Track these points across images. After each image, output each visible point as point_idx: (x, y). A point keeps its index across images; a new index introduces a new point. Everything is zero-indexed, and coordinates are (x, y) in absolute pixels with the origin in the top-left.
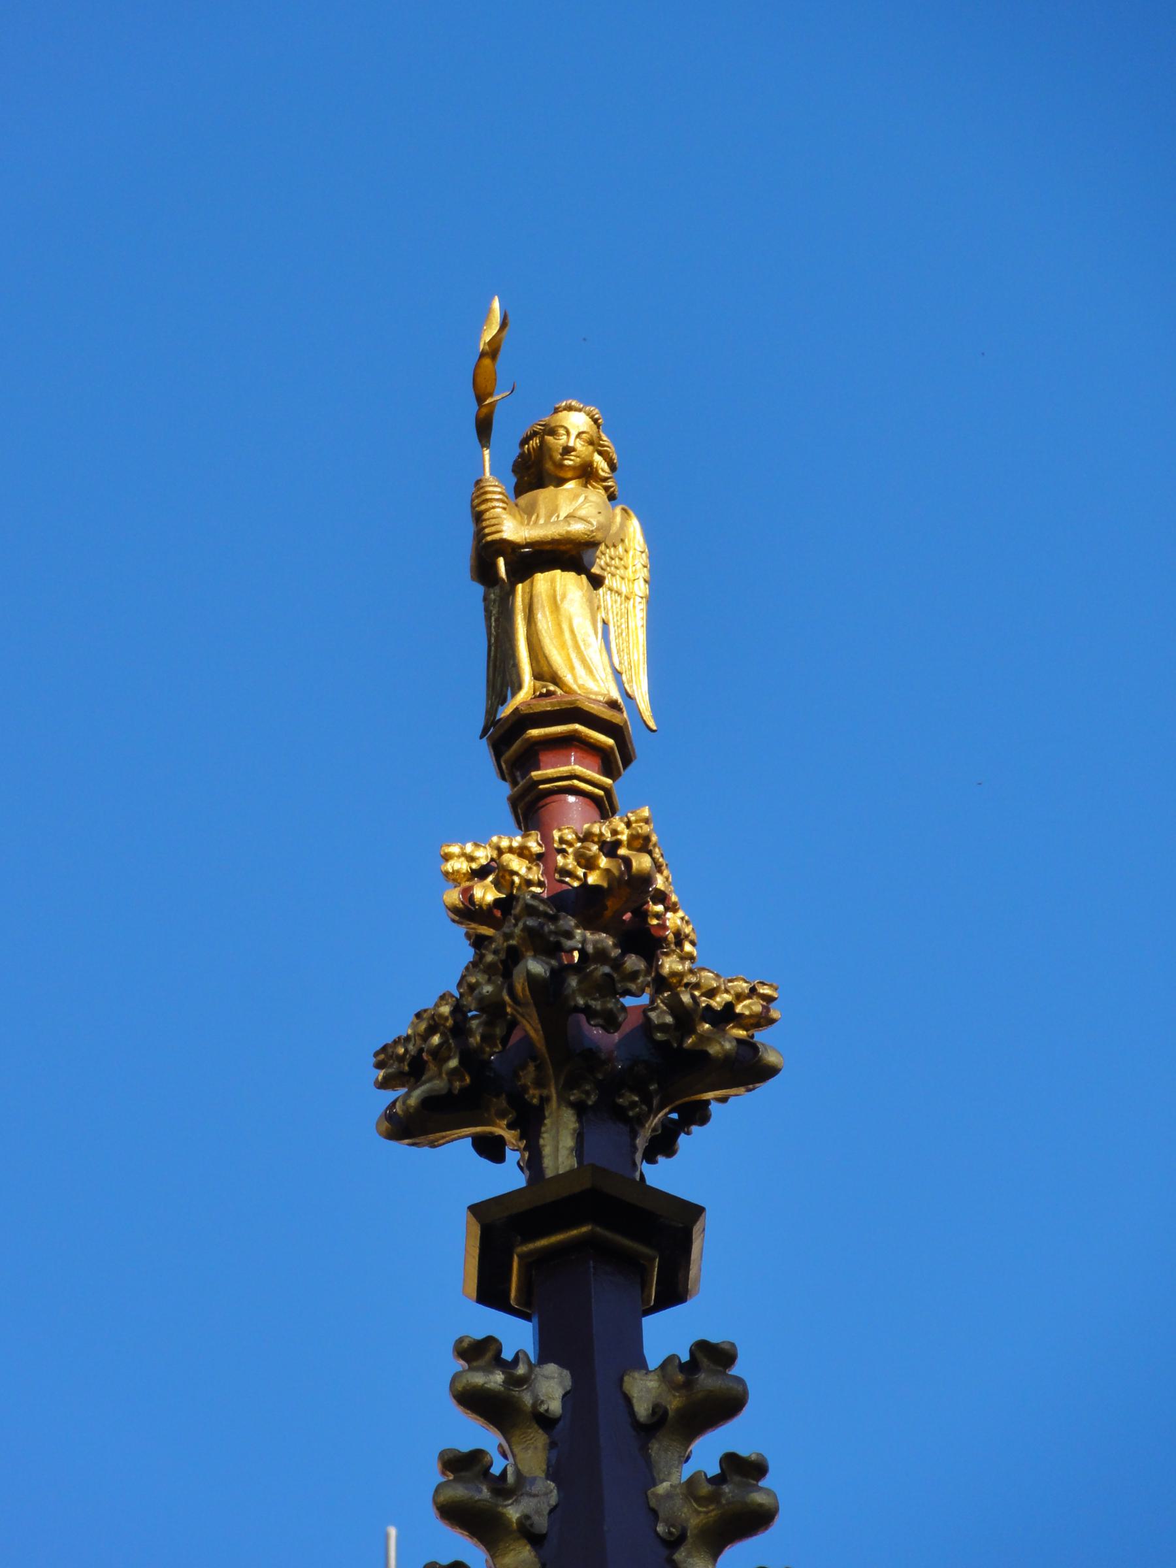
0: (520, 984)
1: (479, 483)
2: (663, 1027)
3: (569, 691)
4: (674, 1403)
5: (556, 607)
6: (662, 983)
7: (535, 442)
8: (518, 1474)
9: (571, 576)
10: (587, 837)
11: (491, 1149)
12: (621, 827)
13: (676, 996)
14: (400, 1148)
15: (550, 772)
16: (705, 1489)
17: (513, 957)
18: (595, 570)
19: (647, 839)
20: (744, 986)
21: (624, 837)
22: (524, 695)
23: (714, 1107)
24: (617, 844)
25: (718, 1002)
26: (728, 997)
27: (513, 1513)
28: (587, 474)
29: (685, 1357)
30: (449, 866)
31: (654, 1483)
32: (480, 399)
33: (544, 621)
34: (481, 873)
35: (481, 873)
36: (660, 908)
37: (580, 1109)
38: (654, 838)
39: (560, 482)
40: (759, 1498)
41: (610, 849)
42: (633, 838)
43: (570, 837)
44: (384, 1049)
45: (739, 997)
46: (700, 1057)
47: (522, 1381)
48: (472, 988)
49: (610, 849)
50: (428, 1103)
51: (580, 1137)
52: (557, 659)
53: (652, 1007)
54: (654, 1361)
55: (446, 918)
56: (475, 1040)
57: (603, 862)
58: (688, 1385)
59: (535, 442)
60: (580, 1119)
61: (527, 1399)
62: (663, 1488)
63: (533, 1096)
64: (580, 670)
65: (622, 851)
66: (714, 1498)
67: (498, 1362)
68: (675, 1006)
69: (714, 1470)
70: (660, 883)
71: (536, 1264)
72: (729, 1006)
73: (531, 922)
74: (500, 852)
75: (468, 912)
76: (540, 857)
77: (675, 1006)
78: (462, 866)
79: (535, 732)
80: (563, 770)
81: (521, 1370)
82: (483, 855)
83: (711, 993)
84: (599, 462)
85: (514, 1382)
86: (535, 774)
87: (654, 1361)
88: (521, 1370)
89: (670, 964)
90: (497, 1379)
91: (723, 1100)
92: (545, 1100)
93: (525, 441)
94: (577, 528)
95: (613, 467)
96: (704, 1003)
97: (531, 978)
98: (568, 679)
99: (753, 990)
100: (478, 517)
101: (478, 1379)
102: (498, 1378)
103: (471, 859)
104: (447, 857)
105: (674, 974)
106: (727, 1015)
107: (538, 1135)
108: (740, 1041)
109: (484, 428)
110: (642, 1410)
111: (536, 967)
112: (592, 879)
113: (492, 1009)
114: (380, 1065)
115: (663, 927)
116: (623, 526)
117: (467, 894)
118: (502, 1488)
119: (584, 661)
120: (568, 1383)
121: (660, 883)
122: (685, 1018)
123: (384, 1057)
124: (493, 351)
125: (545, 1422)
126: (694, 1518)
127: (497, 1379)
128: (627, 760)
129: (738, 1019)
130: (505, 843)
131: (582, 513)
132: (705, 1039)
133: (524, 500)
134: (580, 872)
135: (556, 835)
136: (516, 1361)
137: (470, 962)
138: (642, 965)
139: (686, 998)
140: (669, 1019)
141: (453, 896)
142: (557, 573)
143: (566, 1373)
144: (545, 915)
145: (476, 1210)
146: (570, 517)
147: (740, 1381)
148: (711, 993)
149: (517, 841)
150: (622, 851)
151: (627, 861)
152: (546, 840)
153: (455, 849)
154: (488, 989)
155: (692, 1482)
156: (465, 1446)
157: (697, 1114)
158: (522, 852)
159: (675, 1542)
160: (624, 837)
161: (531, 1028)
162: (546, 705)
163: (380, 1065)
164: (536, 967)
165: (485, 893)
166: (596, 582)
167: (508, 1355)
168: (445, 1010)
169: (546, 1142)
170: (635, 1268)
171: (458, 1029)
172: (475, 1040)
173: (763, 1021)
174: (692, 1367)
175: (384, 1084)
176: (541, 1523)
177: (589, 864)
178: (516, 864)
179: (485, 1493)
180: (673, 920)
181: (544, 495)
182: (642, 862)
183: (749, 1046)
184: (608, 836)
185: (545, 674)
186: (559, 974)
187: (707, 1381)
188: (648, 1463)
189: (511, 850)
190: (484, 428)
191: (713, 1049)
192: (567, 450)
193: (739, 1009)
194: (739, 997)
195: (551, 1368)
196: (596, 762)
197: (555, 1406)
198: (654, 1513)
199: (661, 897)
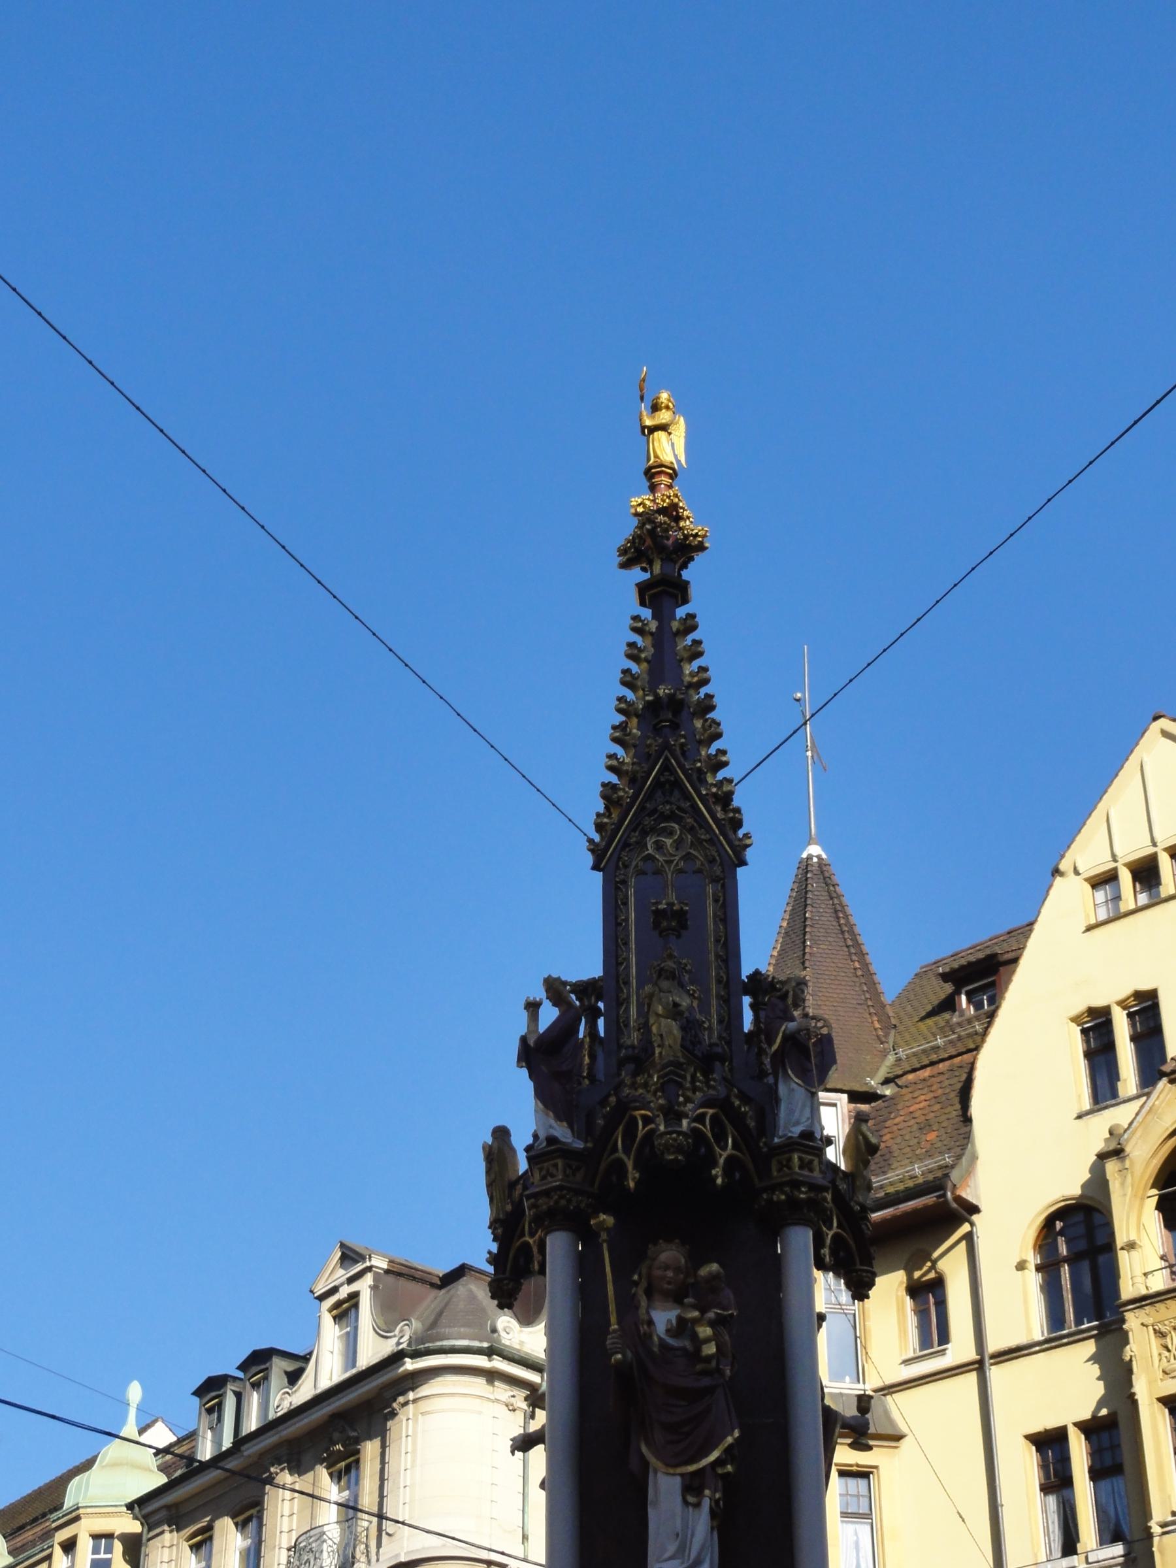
0: (645, 531)
1: (641, 413)
2: (680, 539)
3: (661, 460)
4: (682, 628)
5: (659, 441)
6: (681, 529)
7: (655, 401)
8: (644, 647)
9: (663, 433)
10: (663, 495)
11: (644, 570)
12: (671, 492)
13: (683, 532)
14: (623, 571)
15: (656, 480)
16: (688, 648)
17: (644, 524)
18: (669, 431)
19: (677, 495)
20: (700, 528)
21: (672, 495)
22: (651, 462)
23: (695, 557)
24: (670, 496)
25: (694, 532)
26: (696, 531)
27: (643, 656)
28: (667, 408)
29: (684, 617)
30: (632, 504)
31: (677, 646)
32: (641, 391)
33: (656, 444)
34: (639, 505)
35: (639, 505)
36: (682, 511)
37: (662, 560)
38: (679, 494)
39: (661, 410)
40: (700, 649)
41: (669, 497)
42: (674, 494)
43: (659, 495)
44: (619, 548)
45: (699, 531)
46: (690, 545)
47: (647, 624)
48: (636, 532)
49: (669, 497)
50: (628, 560)
51: (662, 566)
52: (659, 453)
53: (678, 534)
54: (678, 619)
55: (632, 516)
56: (637, 545)
57: (667, 501)
58: (685, 623)
59: (655, 401)
60: (661, 561)
61: (647, 629)
62: (678, 648)
63: (651, 557)
64: (664, 455)
65: (672, 498)
66: (690, 650)
67: (641, 621)
68: (683, 534)
69: (690, 643)
70: (681, 504)
71: (652, 597)
72: (697, 533)
73: (647, 516)
74: (644, 500)
75: (636, 514)
76: (652, 500)
77: (683, 534)
78: (635, 503)
79: (653, 471)
80: (660, 479)
81: (646, 622)
82: (640, 501)
83: (692, 530)
84: (670, 405)
85: (644, 625)
86: (653, 481)
87: (678, 619)
88: (646, 622)
89: (682, 524)
90: (640, 624)
91: (697, 555)
92: (654, 558)
93: (653, 401)
94: (664, 421)
95: (674, 406)
96: (691, 533)
97: (648, 530)
98: (661, 457)
99: (703, 529)
100: (641, 420)
101: (635, 625)
102: (641, 624)
103: (637, 502)
104: (631, 502)
105: (683, 526)
106: (696, 535)
107: (652, 566)
108: (699, 541)
109: (642, 398)
110: (674, 629)
111: (648, 527)
112: (665, 505)
113: (640, 537)
114: (618, 551)
115: (683, 515)
116: (679, 420)
117: (636, 510)
118: (640, 650)
119: (666, 453)
120: (657, 624)
121: (681, 504)
122: (686, 537)
123: (619, 550)
124: (644, 380)
125: (652, 634)
126: (686, 655)
127: (640, 624)
128: (676, 475)
129: (699, 536)
130: (644, 498)
131: (666, 417)
132: (691, 541)
133: (653, 414)
134: (662, 503)
135: (656, 495)
136: (644, 620)
137: (636, 527)
138: (675, 525)
139: (686, 532)
140: (682, 537)
141: (633, 511)
142: (660, 432)
143: (657, 622)
144: (651, 514)
145: (637, 585)
146: (662, 419)
147: (697, 622)
148: (692, 530)
149: (647, 497)
150: (672, 498)
151: (672, 500)
152: (654, 496)
153: (633, 499)
154: (639, 532)
155: (685, 647)
156: (632, 641)
157: (692, 559)
158: (649, 499)
159: (681, 660)
160: (672, 495)
161: (649, 542)
162: (656, 464)
163: (618, 551)
164: (648, 527)
165: (640, 510)
166: (670, 434)
167: (643, 618)
168: (631, 538)
169: (654, 567)
170: (676, 597)
171: (633, 542)
172: (637, 545)
173: (704, 536)
174: (685, 620)
175: (619, 556)
176: (650, 658)
177: (664, 501)
178: (648, 503)
179: (636, 651)
180: (686, 513)
181: (657, 413)
182: (676, 500)
183: (701, 543)
184: (668, 494)
185: (656, 456)
186: (654, 529)
187: (689, 622)
188: (675, 642)
189: (646, 499)
190: (642, 398)
191: (693, 544)
192: (662, 403)
193: (699, 534)
194: (699, 531)
195: (654, 621)
196: (668, 477)
197: (654, 630)
198: (676, 654)
199: (682, 508)
